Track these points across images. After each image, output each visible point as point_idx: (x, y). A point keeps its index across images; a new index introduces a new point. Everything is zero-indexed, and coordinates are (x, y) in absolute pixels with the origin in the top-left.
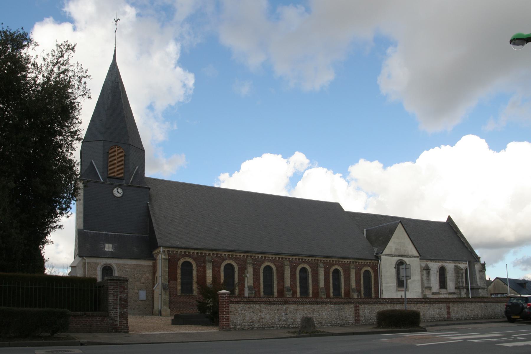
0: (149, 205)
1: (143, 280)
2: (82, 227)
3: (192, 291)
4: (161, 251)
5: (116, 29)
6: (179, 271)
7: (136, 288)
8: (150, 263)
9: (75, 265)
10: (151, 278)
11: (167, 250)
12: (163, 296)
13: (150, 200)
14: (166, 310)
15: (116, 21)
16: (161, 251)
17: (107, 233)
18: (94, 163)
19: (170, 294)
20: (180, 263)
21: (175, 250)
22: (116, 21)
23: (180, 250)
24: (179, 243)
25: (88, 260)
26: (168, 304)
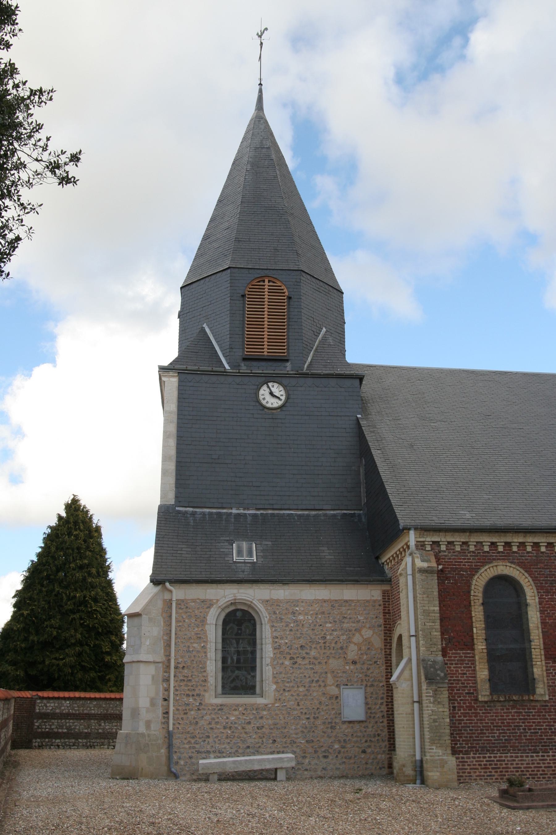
0: (362, 423)
1: (352, 652)
2: (171, 500)
3: (527, 684)
4: (412, 543)
5: (261, 44)
6: (478, 613)
7: (330, 680)
8: (372, 593)
9: (137, 610)
10: (378, 642)
11: (429, 539)
12: (429, 707)
13: (364, 409)
14: (443, 764)
15: (260, 36)
16: (412, 543)
17: (241, 511)
18: (208, 330)
19: (451, 700)
20: (479, 582)
21: (458, 538)
22: (260, 36)
23: (474, 539)
24: (468, 516)
25: (178, 593)
26: (447, 739)
